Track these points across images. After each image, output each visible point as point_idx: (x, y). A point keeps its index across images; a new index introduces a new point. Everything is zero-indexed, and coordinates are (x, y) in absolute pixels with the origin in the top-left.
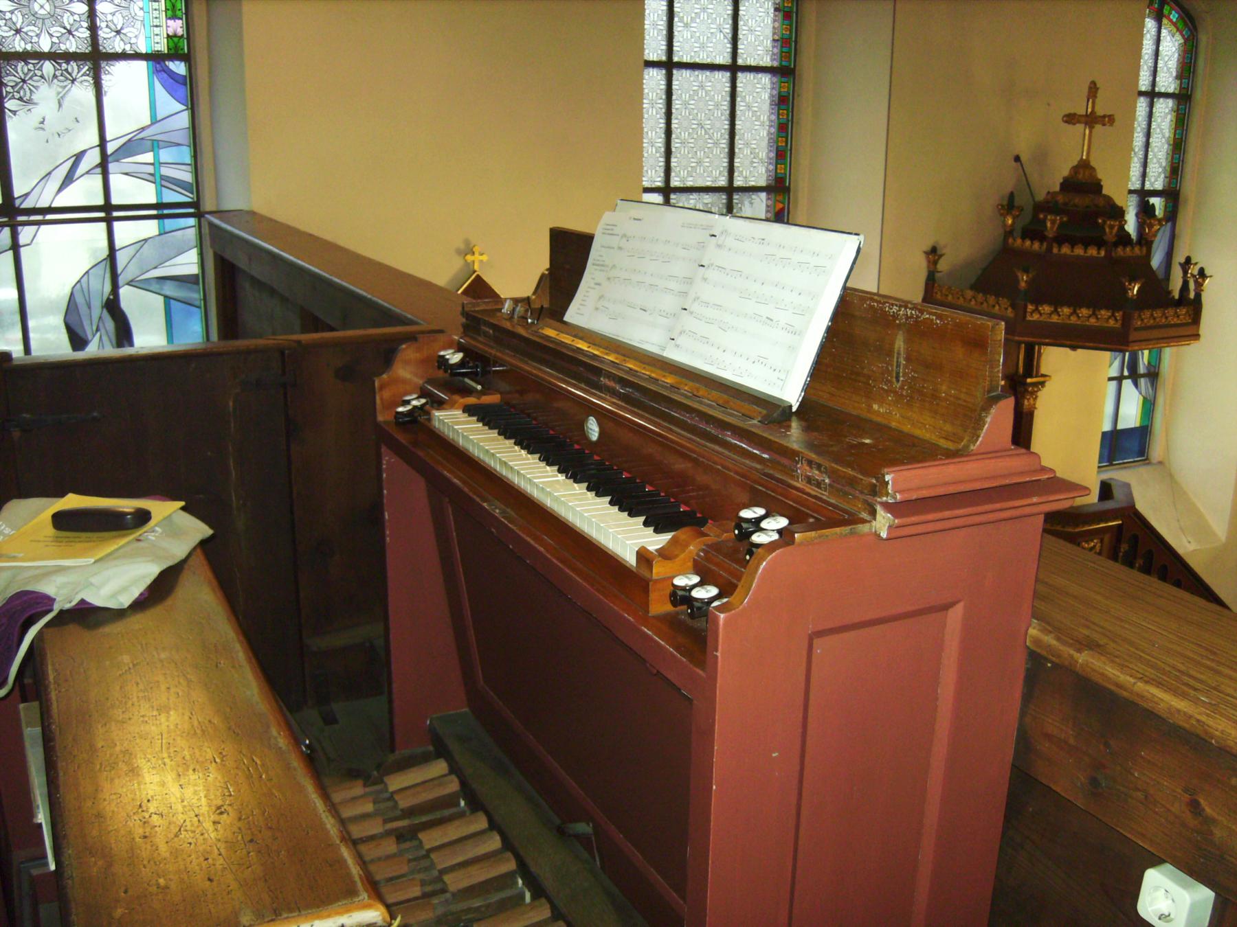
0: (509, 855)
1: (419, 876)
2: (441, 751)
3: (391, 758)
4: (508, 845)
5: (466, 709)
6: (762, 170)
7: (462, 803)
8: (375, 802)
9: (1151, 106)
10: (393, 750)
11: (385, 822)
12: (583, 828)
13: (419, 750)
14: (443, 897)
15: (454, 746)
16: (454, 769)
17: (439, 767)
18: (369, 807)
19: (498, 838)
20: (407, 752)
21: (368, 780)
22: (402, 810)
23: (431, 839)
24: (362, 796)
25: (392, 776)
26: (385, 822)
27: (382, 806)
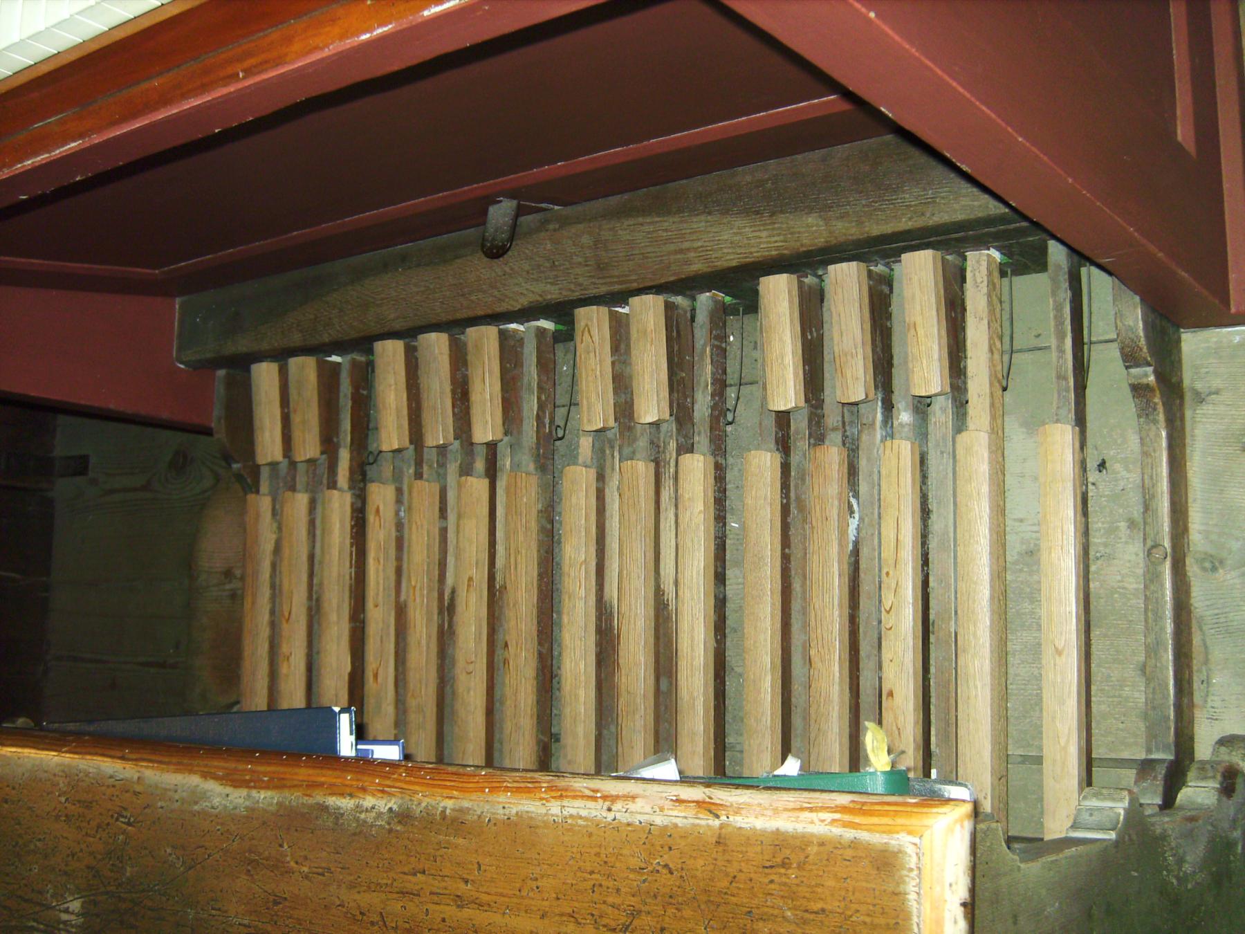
0: (472, 332)
1: (452, 468)
2: (242, 364)
3: (221, 434)
4: (454, 326)
5: (178, 300)
6: (755, 462)
7: (335, 358)
8: (293, 489)
9: (867, 396)
10: (208, 432)
11: (333, 485)
12: (501, 213)
13: (220, 390)
14: (503, 450)
15: (243, 345)
16: (281, 356)
17: (265, 375)
18: (302, 499)
19: (433, 335)
20: (217, 411)
21: (249, 480)
22: (322, 453)
23: (391, 432)
24: (274, 501)
25: (259, 450)
26: (333, 485)
27: (301, 479)
